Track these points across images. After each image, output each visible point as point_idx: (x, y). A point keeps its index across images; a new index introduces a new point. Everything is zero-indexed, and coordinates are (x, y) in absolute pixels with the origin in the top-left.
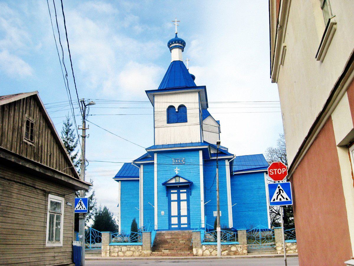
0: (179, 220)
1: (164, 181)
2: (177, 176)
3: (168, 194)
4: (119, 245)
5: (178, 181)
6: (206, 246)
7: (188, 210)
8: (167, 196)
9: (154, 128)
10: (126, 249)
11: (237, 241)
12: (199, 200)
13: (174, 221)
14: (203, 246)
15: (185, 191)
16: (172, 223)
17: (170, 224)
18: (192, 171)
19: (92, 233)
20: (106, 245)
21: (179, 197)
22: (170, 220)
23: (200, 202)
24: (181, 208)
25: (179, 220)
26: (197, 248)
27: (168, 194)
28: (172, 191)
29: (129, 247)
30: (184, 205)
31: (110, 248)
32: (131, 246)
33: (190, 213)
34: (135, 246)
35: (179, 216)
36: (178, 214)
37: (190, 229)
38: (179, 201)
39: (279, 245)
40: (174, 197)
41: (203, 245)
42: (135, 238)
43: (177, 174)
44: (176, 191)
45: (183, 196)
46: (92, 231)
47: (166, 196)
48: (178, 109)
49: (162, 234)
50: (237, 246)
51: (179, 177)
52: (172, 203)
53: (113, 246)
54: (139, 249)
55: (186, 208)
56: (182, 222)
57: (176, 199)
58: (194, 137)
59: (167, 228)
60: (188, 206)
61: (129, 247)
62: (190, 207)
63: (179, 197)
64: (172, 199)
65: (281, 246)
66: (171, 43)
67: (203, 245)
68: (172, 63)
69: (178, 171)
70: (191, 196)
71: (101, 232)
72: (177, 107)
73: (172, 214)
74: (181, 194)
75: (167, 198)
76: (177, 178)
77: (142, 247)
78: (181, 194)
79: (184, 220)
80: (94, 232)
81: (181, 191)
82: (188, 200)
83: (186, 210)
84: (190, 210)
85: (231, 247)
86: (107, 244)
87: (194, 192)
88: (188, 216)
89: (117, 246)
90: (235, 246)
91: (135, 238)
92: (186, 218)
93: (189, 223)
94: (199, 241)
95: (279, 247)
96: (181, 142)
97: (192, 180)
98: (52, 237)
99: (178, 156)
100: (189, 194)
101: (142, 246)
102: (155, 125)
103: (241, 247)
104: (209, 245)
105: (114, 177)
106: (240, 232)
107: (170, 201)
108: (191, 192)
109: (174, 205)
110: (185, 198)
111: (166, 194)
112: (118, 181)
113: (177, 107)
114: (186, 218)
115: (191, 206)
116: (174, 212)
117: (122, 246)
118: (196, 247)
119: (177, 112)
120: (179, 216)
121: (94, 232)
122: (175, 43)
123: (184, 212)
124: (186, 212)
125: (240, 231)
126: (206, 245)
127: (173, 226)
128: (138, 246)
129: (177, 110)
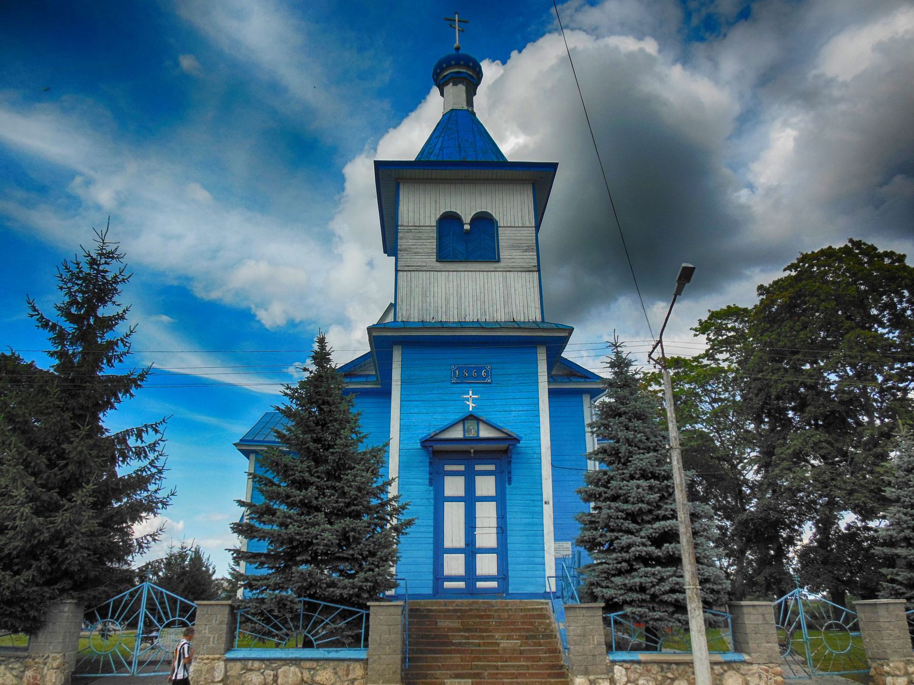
0: (470, 565)
1: (424, 433)
2: (472, 417)
3: (436, 479)
4: (269, 660)
5: (472, 434)
6: (626, 669)
7: (502, 530)
8: (431, 484)
9: (397, 271)
10: (295, 674)
11: (738, 649)
12: (539, 497)
13: (454, 565)
14: (617, 668)
15: (492, 467)
16: (447, 571)
17: (439, 576)
18: (513, 408)
19: (152, 608)
20: (211, 657)
21: (470, 487)
22: (438, 564)
23: (542, 507)
24: (479, 523)
25: (470, 565)
26: (592, 677)
27: (436, 479)
28: (448, 468)
29: (310, 669)
30: (487, 514)
31: (226, 672)
32: (321, 663)
33: (508, 541)
34: (336, 663)
35: (471, 550)
36: (467, 545)
37: (508, 594)
38: (470, 500)
39: (898, 669)
40: (454, 486)
41: (614, 662)
42: (327, 621)
43: (471, 409)
44: (461, 468)
45: (486, 485)
46: (150, 599)
47: (427, 482)
48: (471, 224)
49: (425, 613)
50: (744, 668)
51: (478, 420)
52: (447, 505)
53: (239, 665)
54: (351, 676)
55: (494, 522)
56: (480, 571)
57: (461, 492)
58: (521, 305)
59: (429, 591)
60: (502, 517)
61: (310, 669)
62: (506, 521)
63: (470, 487)
64: (448, 492)
65: (903, 672)
66: (453, 62)
67: (614, 662)
68: (448, 116)
69: (474, 400)
70: (510, 484)
71: (195, 604)
72: (467, 218)
73: (447, 544)
74: (461, 571)
75: (431, 488)
76: (471, 425)
77: (366, 669)
78: (461, 571)
79: (487, 565)
80: (162, 603)
81: (478, 468)
82: (500, 499)
83: (495, 530)
84: (508, 532)
85: (722, 674)
86: (217, 656)
87: (518, 473)
88: (501, 551)
89: (256, 664)
90: (738, 670)
91: (327, 621)
92: (494, 557)
93: (503, 576)
94: (599, 644)
95: (898, 676)
96: (479, 317)
97: (515, 431)
98: (494, 650)
99: (472, 357)
100: (504, 478)
101: (365, 662)
102: (399, 264)
103: (760, 677)
104: (639, 662)
105: (238, 441)
106: (750, 614)
107: (439, 500)
108: (510, 473)
109: (454, 514)
110: (492, 492)
111: (427, 476)
112: (247, 453)
113: (467, 218)
114: (494, 557)
115: (510, 518)
116: (454, 535)
117: (280, 663)
118: (586, 673)
119: (467, 232)
120: (471, 550)
121: (162, 603)
122: (458, 65)
123: (487, 537)
124: (494, 537)
125: (751, 610)
126: (628, 665)
127: (447, 585)
128: (348, 666)
129: (467, 227)
